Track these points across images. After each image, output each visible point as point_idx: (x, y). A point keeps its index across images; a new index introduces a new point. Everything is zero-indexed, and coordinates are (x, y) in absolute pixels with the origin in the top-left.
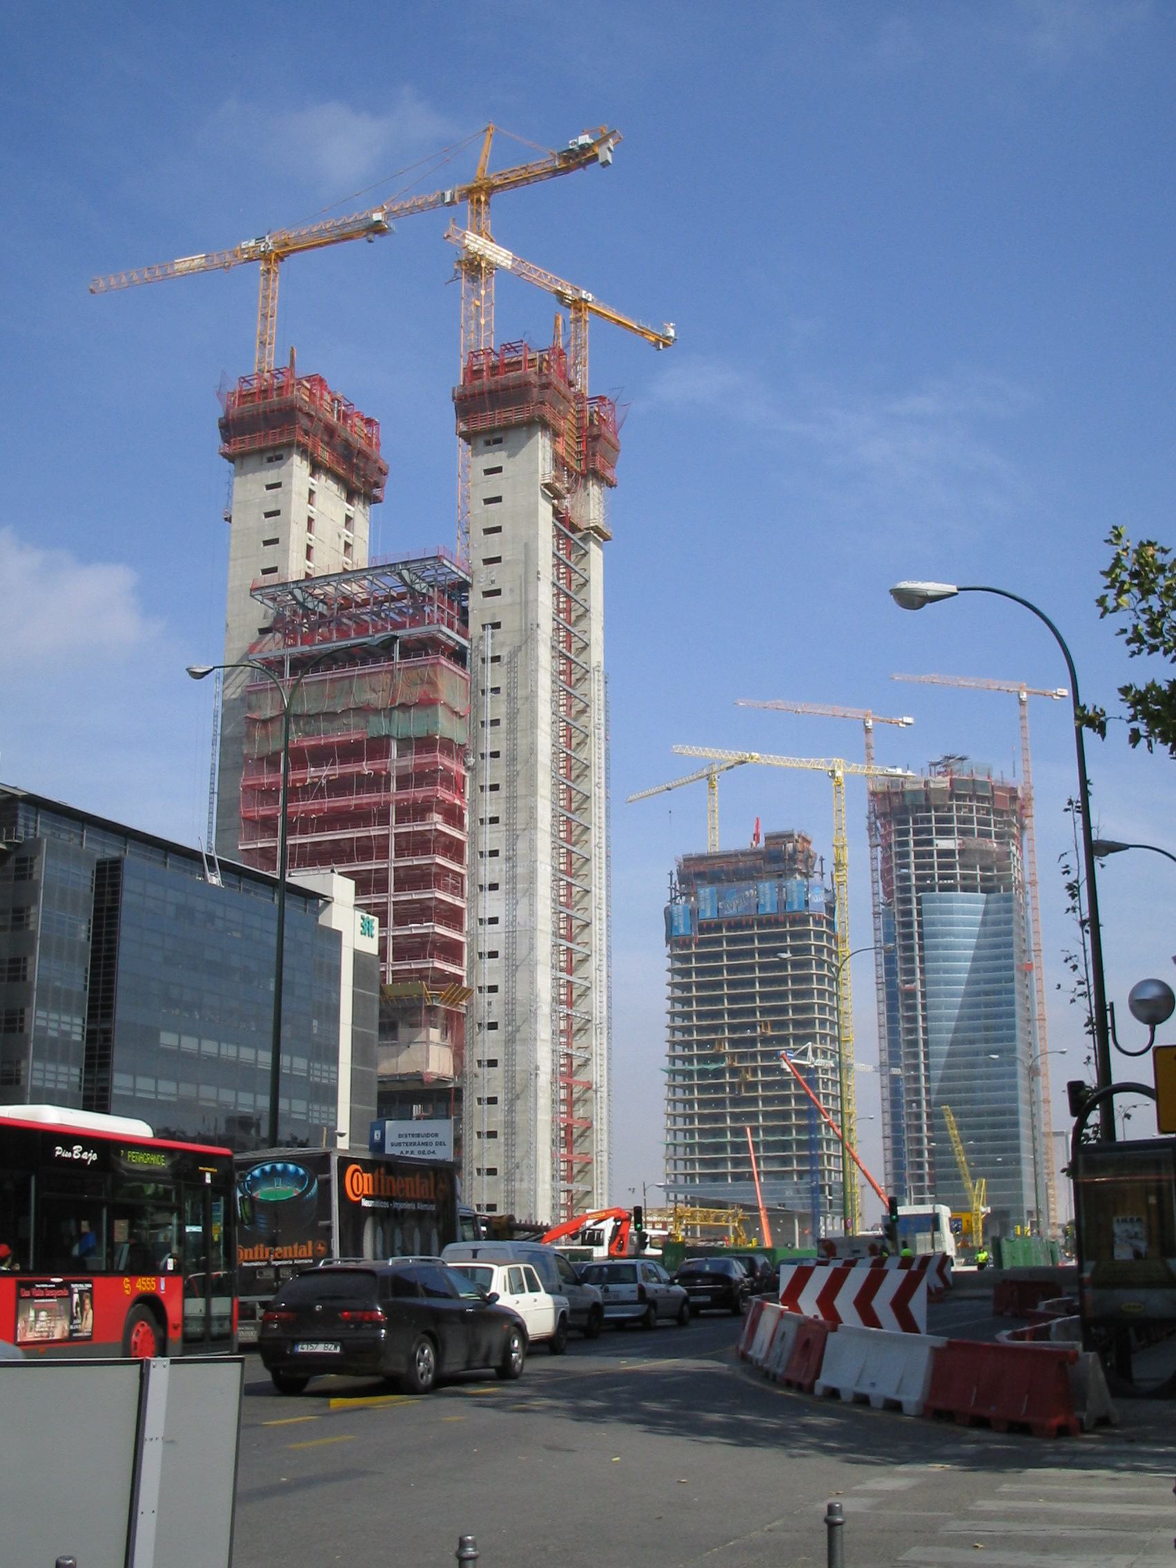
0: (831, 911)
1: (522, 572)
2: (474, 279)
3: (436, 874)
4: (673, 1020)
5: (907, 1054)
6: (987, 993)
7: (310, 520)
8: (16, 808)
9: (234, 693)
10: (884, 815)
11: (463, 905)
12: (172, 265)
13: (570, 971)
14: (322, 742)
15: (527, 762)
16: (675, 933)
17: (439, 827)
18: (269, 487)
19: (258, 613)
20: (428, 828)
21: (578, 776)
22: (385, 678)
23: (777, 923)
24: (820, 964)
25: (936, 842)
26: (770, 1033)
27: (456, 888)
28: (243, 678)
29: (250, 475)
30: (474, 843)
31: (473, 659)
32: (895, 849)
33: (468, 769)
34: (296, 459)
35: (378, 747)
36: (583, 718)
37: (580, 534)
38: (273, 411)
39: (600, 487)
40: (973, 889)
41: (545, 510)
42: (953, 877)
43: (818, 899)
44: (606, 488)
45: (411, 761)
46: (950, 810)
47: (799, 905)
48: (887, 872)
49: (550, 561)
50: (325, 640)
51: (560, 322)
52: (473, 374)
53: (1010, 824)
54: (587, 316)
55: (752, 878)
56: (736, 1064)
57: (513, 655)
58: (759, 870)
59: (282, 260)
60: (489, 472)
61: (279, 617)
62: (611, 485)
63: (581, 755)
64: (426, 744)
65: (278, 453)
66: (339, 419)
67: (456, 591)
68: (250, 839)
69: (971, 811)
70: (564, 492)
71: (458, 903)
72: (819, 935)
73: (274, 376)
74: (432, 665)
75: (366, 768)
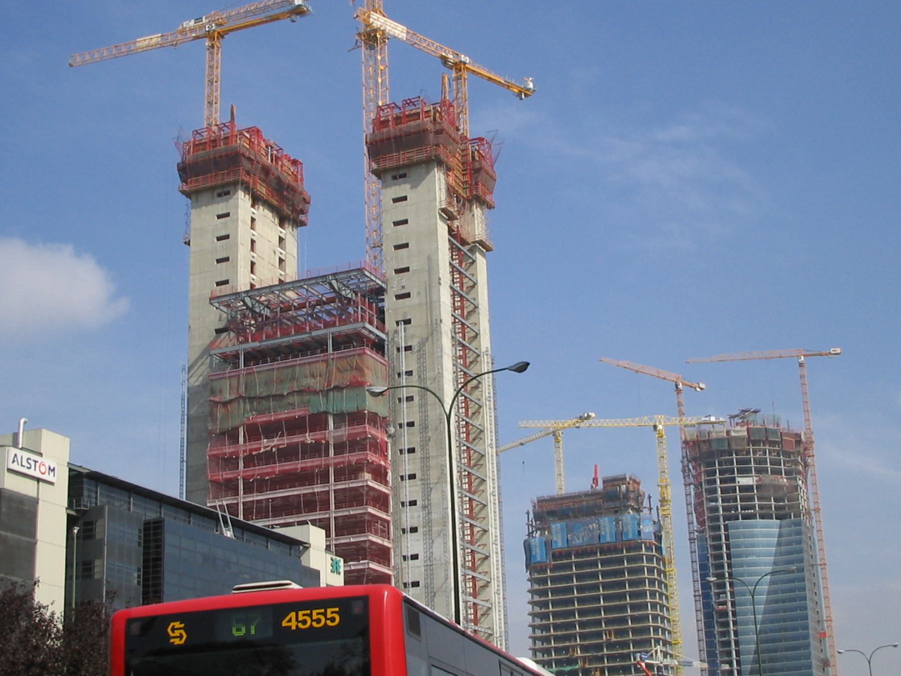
0: (659, 538)
2: (372, 48)
3: (369, 521)
4: (534, 631)
5: (721, 652)
6: (784, 601)
7: (253, 242)
8: (82, 483)
9: (196, 381)
10: (694, 459)
11: (390, 545)
12: (135, 43)
13: (475, 595)
14: (273, 419)
15: (437, 429)
16: (533, 561)
17: (370, 483)
18: (219, 217)
19: (215, 317)
20: (360, 484)
21: (474, 439)
22: (322, 367)
23: (616, 550)
25: (738, 479)
26: (613, 639)
27: (383, 531)
28: (203, 370)
29: (204, 208)
30: (396, 495)
31: (390, 349)
33: (390, 436)
34: (241, 194)
35: (318, 422)
36: (477, 393)
37: (468, 247)
38: (221, 157)
39: (482, 210)
40: (770, 517)
41: (442, 229)
43: (648, 529)
44: (486, 210)
45: (345, 432)
46: (748, 453)
47: (633, 535)
48: (699, 505)
49: (448, 269)
50: (269, 337)
51: (446, 80)
52: (380, 124)
53: (796, 463)
54: (466, 75)
55: (594, 514)
56: (587, 666)
57: (422, 344)
58: (600, 507)
59: (223, 37)
60: (396, 200)
61: (232, 320)
62: (490, 207)
63: (476, 423)
64: (357, 417)
65: (226, 190)
66: (272, 160)
67: (373, 296)
68: (216, 497)
69: (765, 453)
70: (455, 214)
71: (386, 544)
72: (650, 559)
73: (220, 129)
74: (359, 355)
75: (309, 438)
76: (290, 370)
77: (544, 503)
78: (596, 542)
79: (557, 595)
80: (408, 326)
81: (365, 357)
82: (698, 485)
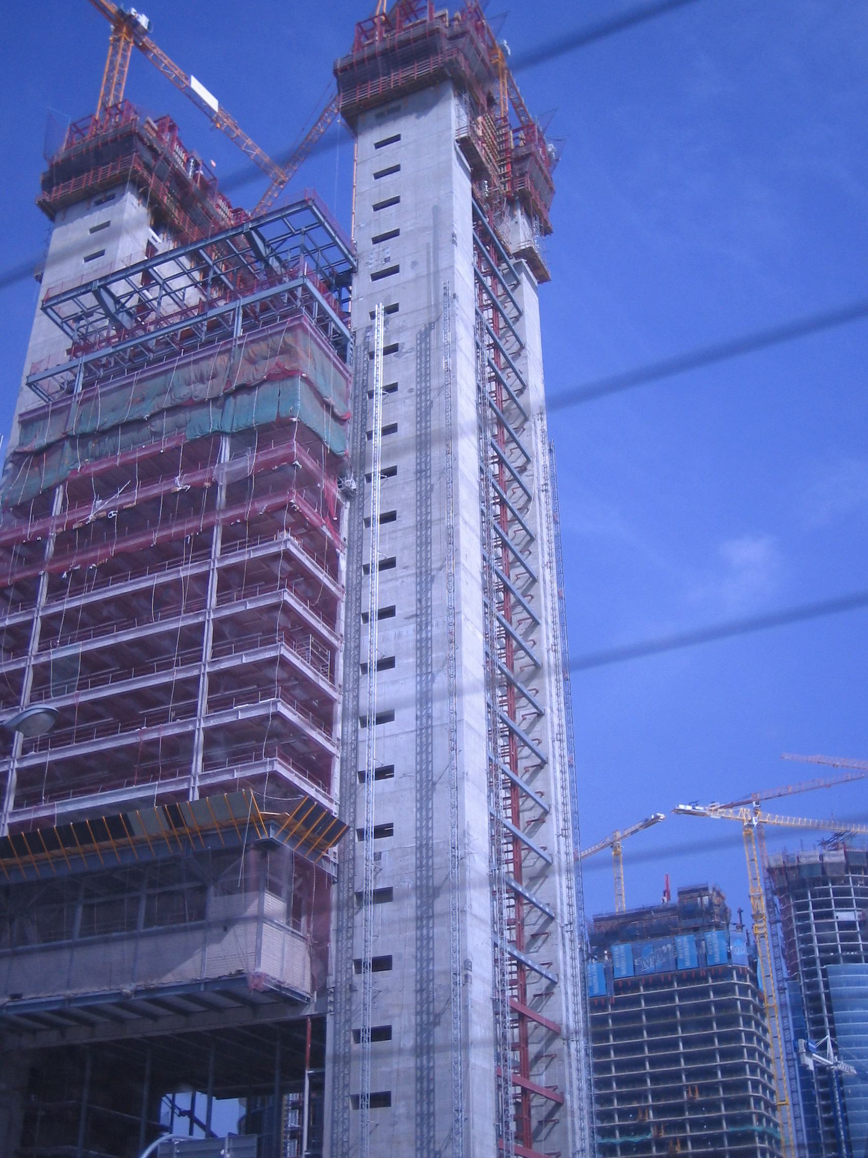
0: (754, 965)
1: (430, 240)
5: (825, 1132)
24: (747, 1023)
26: (698, 1098)
32: (795, 923)
38: (105, 144)
42: (856, 948)
43: (739, 951)
46: (847, 882)
56: (663, 1135)
65: (109, 194)
76: (162, 378)
77: (603, 923)
78: (672, 968)
79: (621, 1039)
80: (393, 315)
81: (299, 332)
82: (787, 923)
